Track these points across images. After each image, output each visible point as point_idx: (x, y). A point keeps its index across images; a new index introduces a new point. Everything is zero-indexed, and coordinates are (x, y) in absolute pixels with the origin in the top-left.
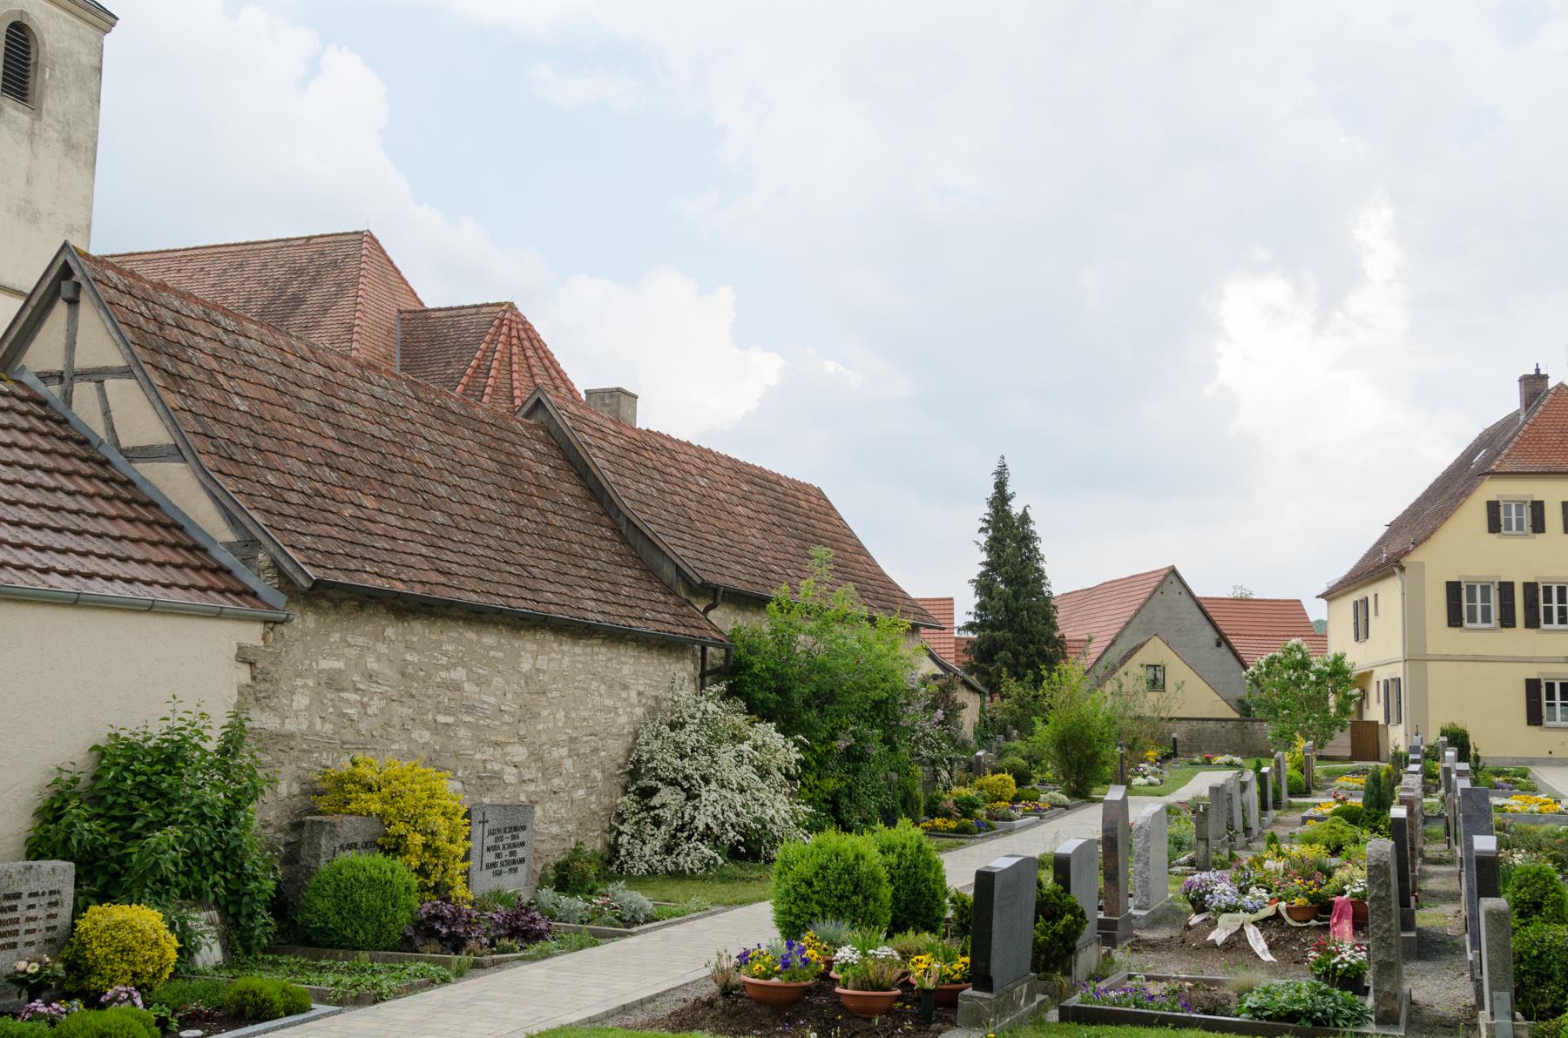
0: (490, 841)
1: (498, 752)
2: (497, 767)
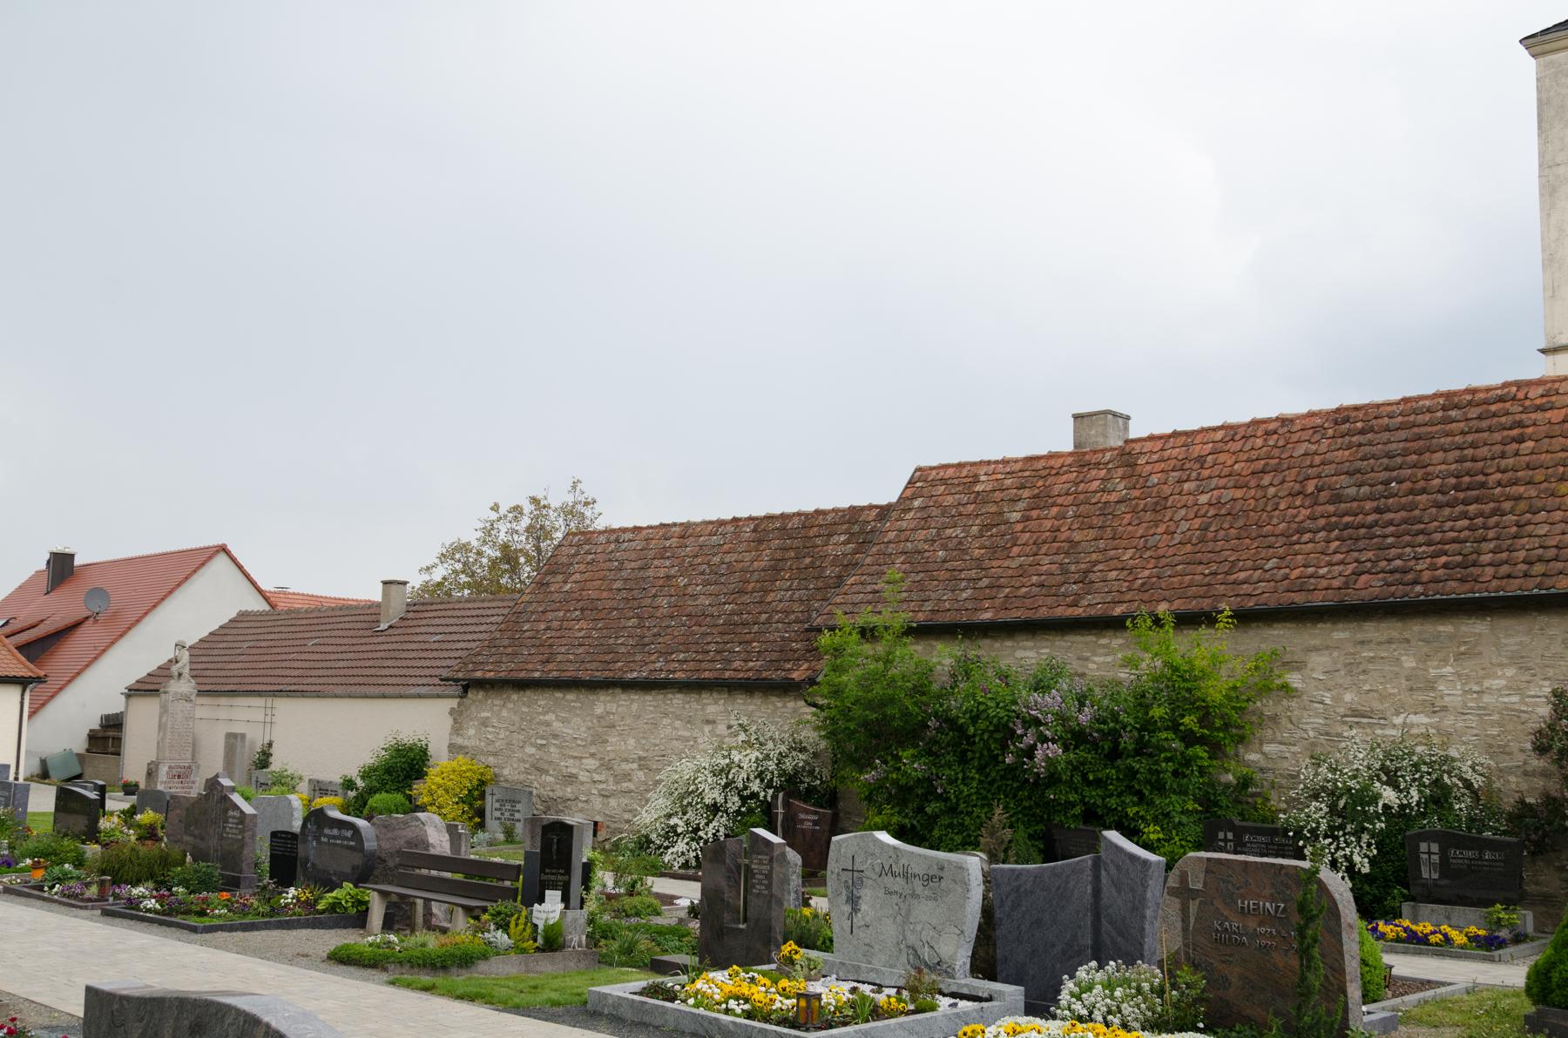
0: (497, 805)
1: (577, 762)
2: (574, 771)
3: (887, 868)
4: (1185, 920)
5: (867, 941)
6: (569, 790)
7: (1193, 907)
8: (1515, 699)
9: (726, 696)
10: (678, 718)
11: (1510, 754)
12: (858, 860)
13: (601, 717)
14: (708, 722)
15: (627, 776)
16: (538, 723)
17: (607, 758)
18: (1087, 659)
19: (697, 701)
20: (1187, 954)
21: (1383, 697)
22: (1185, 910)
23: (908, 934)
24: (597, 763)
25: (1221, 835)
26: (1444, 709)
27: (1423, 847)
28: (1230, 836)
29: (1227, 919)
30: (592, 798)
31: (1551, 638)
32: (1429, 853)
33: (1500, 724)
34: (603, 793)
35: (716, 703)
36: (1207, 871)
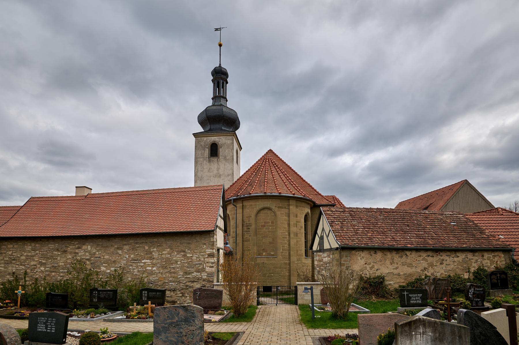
8: (169, 256)
18: (68, 247)
25: (94, 292)
26: (154, 258)
28: (96, 292)
33: (165, 261)
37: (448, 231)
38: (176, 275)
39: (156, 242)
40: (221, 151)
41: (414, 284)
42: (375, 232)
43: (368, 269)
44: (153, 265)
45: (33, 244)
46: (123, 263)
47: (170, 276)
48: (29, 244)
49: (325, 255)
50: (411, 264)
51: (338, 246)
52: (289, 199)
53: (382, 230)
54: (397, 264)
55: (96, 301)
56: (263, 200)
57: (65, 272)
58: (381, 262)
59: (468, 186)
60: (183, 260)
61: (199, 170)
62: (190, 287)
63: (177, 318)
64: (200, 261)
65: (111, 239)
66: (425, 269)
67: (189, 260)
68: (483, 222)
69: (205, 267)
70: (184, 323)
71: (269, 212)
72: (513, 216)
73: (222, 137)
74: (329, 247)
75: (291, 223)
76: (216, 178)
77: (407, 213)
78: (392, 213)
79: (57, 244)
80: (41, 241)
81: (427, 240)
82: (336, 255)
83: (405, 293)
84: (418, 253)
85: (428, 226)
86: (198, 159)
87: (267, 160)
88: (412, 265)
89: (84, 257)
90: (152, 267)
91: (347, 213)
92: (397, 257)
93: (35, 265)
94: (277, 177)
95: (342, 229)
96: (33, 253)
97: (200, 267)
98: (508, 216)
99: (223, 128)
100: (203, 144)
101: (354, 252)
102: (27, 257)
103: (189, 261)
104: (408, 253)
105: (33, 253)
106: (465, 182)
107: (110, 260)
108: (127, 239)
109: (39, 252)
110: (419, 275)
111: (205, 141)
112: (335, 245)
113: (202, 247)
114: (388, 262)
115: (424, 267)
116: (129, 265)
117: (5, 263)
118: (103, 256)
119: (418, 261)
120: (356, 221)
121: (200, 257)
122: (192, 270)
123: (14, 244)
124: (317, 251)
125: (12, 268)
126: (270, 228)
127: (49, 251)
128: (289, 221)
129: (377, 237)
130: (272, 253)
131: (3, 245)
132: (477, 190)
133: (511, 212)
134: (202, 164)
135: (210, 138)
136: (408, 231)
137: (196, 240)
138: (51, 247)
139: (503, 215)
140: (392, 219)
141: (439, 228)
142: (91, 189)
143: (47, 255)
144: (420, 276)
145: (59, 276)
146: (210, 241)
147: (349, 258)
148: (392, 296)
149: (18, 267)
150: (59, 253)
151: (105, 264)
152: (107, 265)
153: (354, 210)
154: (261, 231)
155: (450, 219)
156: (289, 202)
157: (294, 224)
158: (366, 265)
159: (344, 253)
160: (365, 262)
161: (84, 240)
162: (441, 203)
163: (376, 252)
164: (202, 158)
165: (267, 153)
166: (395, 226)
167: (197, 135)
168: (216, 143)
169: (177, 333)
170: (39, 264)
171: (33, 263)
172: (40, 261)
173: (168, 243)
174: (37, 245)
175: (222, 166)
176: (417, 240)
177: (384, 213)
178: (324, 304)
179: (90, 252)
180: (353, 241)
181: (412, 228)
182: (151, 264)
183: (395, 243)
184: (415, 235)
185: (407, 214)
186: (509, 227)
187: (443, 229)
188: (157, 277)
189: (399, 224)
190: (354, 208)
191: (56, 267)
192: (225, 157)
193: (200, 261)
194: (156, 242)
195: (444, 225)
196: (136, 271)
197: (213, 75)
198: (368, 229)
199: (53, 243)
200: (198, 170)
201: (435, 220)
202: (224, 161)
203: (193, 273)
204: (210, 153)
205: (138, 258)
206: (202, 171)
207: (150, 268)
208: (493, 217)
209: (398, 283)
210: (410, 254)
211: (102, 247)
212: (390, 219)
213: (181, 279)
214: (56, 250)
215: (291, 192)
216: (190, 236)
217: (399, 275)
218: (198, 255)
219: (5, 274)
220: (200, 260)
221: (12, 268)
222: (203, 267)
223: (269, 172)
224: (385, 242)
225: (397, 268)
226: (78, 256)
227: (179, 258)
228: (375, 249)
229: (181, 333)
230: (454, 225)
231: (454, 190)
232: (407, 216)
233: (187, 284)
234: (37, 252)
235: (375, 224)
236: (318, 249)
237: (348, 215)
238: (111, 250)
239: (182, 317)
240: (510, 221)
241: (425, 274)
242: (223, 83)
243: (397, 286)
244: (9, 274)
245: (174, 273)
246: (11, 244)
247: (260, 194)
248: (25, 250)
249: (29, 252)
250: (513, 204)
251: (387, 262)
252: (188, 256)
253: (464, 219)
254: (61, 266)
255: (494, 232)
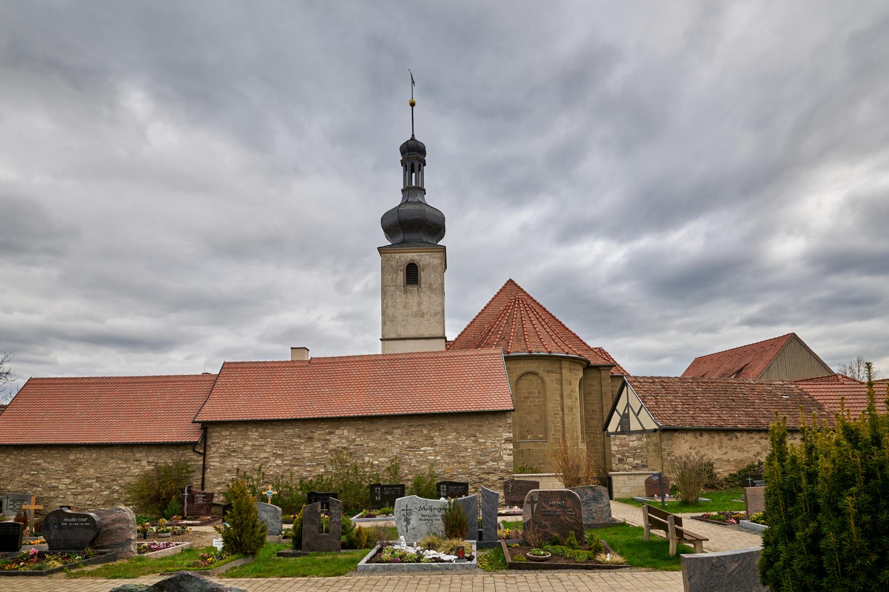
2: (55, 485)
3: (422, 507)
4: (532, 510)
5: (415, 534)
6: (52, 493)
7: (535, 506)
8: (456, 442)
9: (147, 449)
10: (120, 459)
11: (455, 457)
12: (409, 506)
13: (74, 460)
14: (137, 460)
15: (90, 486)
16: (32, 464)
17: (77, 478)
18: (314, 432)
19: (131, 452)
20: (533, 520)
21: (418, 442)
22: (532, 507)
23: (432, 529)
24: (71, 481)
25: (376, 489)
26: (436, 445)
27: (442, 486)
28: (379, 489)
29: (546, 508)
30: (68, 496)
31: (465, 424)
32: (443, 488)
33: (451, 449)
34: (74, 493)
35: (141, 453)
36: (539, 495)
37: (781, 407)
38: (466, 466)
39: (437, 424)
40: (423, 276)
41: (747, 472)
42: (697, 409)
43: (693, 454)
44: (437, 453)
45: (261, 430)
46: (396, 451)
47: (458, 467)
48: (254, 430)
49: (634, 437)
50: (741, 448)
51: (657, 427)
52: (561, 360)
53: (705, 407)
54: (726, 448)
55: (379, 499)
56: (525, 361)
57: (313, 466)
58: (708, 446)
59: (797, 342)
60: (475, 447)
61: (389, 304)
62: (485, 480)
63: (585, 498)
64: (496, 447)
65: (375, 421)
66: (758, 453)
67: (481, 446)
68: (820, 394)
69: (502, 455)
70: (592, 502)
71: (534, 378)
72: (856, 386)
73: (424, 254)
74: (640, 428)
75: (564, 393)
76: (417, 318)
77: (729, 383)
78: (711, 384)
79: (297, 428)
80: (271, 425)
81: (759, 419)
82: (654, 438)
83: (750, 479)
84: (750, 434)
85: (756, 401)
86: (387, 288)
87: (521, 302)
88: (743, 449)
89: (340, 446)
90: (436, 456)
91: (658, 384)
92: (726, 440)
93: (268, 458)
94: (539, 327)
95: (658, 406)
96: (262, 441)
97: (496, 456)
98: (850, 386)
99: (424, 239)
100: (394, 263)
101: (676, 434)
102: (254, 447)
103: (482, 447)
104: (739, 435)
105: (262, 441)
106: (793, 336)
107: (376, 448)
108: (397, 421)
109: (272, 439)
110: (752, 461)
111: (397, 259)
112: (651, 425)
113: (497, 430)
114: (716, 446)
115: (756, 451)
116: (404, 454)
117: (221, 457)
118: (366, 443)
119: (751, 444)
120: (671, 395)
121: (495, 443)
122: (488, 459)
123: (231, 430)
124: (616, 433)
125: (232, 463)
126: (537, 400)
127: (287, 438)
128: (562, 390)
129: (701, 415)
130: (540, 436)
131: (215, 432)
132: (808, 347)
133: (854, 380)
134: (393, 295)
135: (405, 254)
136: (734, 407)
137: (489, 421)
138: (289, 433)
139: (843, 384)
140: (713, 392)
141: (770, 403)
142: (308, 350)
143: (283, 443)
144: (752, 463)
145: (305, 471)
146: (506, 423)
147: (670, 441)
148: (722, 487)
149: (241, 462)
150: (302, 441)
151: (370, 453)
152: (373, 454)
153: (666, 380)
154: (524, 406)
155: (781, 391)
156: (561, 364)
157: (568, 395)
158: (691, 450)
159: (665, 436)
160: (689, 447)
161: (336, 423)
162: (761, 365)
163: (701, 433)
164: (392, 286)
165: (506, 284)
166: (719, 400)
167: (385, 250)
168: (414, 262)
169: (587, 510)
170: (272, 456)
171: (263, 455)
172: (274, 451)
173: (452, 425)
174: (267, 431)
175: (425, 299)
176: (747, 418)
177: (702, 384)
178: (650, 496)
179: (347, 438)
180: (674, 420)
181: (739, 403)
182: (433, 452)
183: (723, 423)
184: (743, 413)
185: (729, 384)
186: (852, 401)
187: (774, 405)
188: (442, 468)
189: (723, 398)
190: (665, 378)
191: (299, 459)
192: (430, 286)
193: (496, 447)
194: (437, 424)
195: (775, 399)
196: (414, 461)
197: (403, 153)
198: (687, 405)
199: (291, 427)
200: (387, 304)
201: (764, 393)
202: (428, 291)
203: (488, 462)
204: (405, 279)
205: (415, 444)
206: (394, 307)
207: (433, 458)
208: (832, 387)
209: (728, 470)
210: (741, 436)
211: (364, 431)
212: (711, 392)
213: (473, 470)
214: (298, 437)
215: (563, 350)
216: (480, 417)
217: (728, 461)
218: (493, 440)
219: (222, 471)
220: (495, 447)
221: (232, 463)
222: (500, 455)
223: (527, 319)
224: (712, 421)
225: (726, 453)
226: (330, 444)
227: (469, 445)
228: (701, 431)
229: (591, 510)
230: (787, 399)
231: (779, 347)
232: (730, 387)
233: (482, 476)
234: (268, 440)
235: (694, 399)
236: (619, 430)
237: (660, 387)
238: (377, 435)
239: (591, 497)
240: (853, 393)
241: (759, 460)
242: (420, 166)
243: (726, 475)
244: (229, 471)
245: (464, 463)
246: (226, 430)
247: (523, 354)
248: (250, 437)
249: (256, 440)
250: (854, 362)
251: (714, 446)
252: (480, 441)
253: (798, 391)
254: (306, 457)
255: (835, 407)
